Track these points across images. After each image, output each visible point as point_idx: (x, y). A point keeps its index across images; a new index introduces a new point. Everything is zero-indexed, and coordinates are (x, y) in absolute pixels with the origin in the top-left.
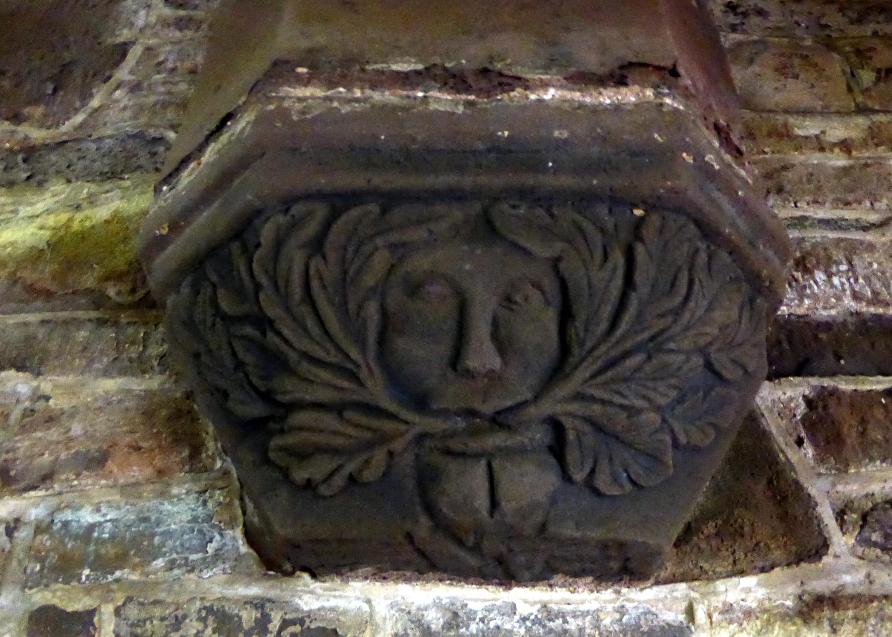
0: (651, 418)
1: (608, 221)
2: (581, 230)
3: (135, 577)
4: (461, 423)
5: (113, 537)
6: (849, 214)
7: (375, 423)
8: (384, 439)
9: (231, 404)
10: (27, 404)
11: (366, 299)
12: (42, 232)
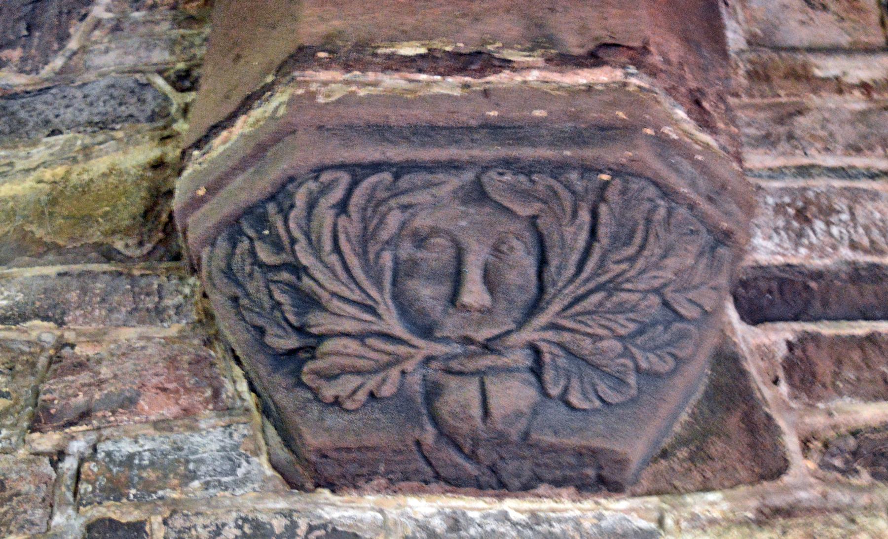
0: (612, 345)
1: (579, 186)
2: (555, 193)
3: (175, 495)
4: (458, 349)
5: (152, 463)
6: (859, 162)
7: (390, 347)
8: (397, 360)
9: (269, 340)
10: (52, 352)
11: (383, 250)
12: (41, 186)
